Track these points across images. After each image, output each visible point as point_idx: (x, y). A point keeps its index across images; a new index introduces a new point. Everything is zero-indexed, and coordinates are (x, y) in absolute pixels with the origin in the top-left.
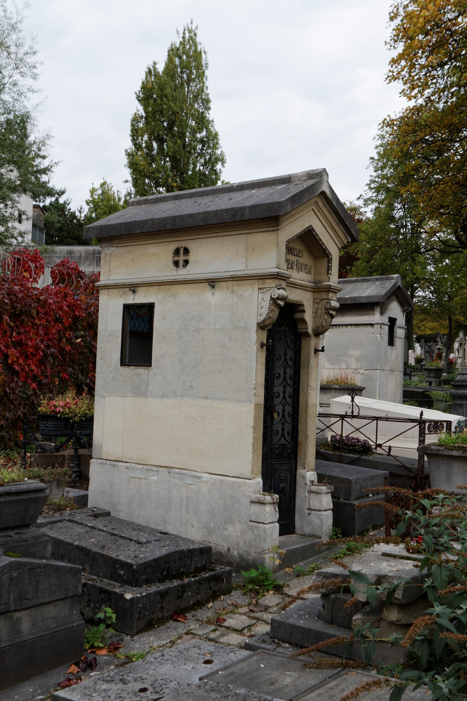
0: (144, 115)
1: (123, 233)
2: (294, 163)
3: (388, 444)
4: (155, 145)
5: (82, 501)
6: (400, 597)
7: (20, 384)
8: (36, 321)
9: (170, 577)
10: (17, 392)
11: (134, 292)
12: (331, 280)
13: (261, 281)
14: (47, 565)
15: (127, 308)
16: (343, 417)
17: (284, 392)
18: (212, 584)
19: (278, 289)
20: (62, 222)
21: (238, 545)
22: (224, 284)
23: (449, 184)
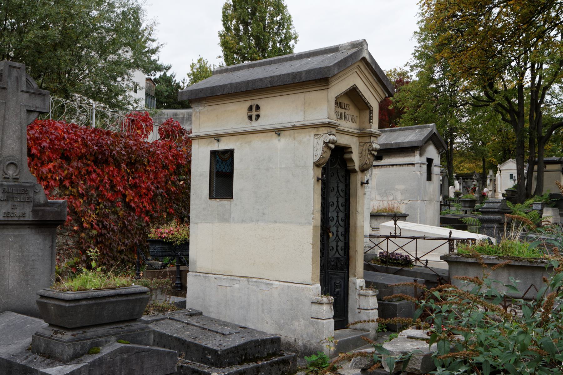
0: (232, 4)
1: (208, 95)
2: (342, 37)
3: (424, 258)
4: (241, 27)
5: (183, 305)
6: (419, 369)
7: (136, 217)
8: (148, 168)
9: (247, 360)
10: (133, 224)
11: (218, 141)
12: (372, 127)
13: (315, 129)
14: (151, 350)
15: (213, 154)
16: (388, 237)
17: (337, 217)
18: (281, 366)
19: (330, 135)
20: (169, 91)
21: (302, 336)
22: (287, 133)
23: (476, 50)
